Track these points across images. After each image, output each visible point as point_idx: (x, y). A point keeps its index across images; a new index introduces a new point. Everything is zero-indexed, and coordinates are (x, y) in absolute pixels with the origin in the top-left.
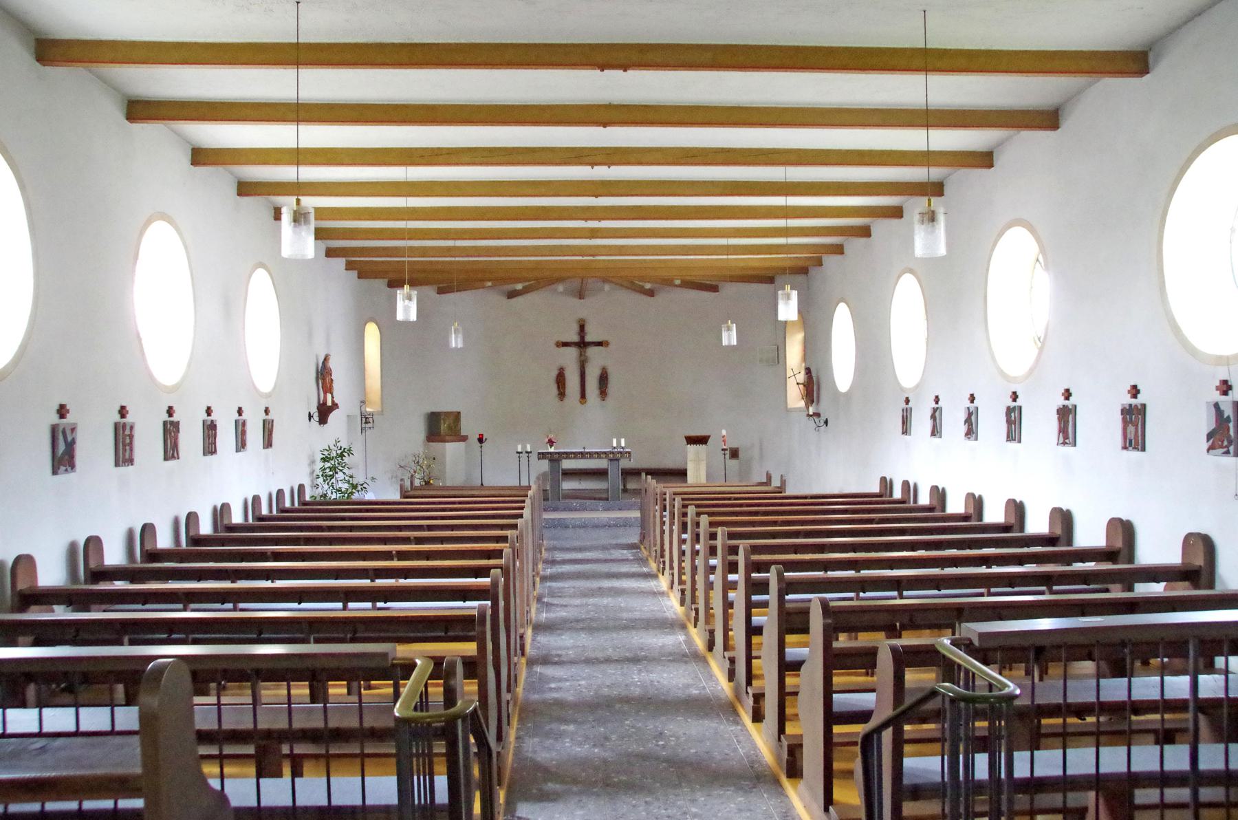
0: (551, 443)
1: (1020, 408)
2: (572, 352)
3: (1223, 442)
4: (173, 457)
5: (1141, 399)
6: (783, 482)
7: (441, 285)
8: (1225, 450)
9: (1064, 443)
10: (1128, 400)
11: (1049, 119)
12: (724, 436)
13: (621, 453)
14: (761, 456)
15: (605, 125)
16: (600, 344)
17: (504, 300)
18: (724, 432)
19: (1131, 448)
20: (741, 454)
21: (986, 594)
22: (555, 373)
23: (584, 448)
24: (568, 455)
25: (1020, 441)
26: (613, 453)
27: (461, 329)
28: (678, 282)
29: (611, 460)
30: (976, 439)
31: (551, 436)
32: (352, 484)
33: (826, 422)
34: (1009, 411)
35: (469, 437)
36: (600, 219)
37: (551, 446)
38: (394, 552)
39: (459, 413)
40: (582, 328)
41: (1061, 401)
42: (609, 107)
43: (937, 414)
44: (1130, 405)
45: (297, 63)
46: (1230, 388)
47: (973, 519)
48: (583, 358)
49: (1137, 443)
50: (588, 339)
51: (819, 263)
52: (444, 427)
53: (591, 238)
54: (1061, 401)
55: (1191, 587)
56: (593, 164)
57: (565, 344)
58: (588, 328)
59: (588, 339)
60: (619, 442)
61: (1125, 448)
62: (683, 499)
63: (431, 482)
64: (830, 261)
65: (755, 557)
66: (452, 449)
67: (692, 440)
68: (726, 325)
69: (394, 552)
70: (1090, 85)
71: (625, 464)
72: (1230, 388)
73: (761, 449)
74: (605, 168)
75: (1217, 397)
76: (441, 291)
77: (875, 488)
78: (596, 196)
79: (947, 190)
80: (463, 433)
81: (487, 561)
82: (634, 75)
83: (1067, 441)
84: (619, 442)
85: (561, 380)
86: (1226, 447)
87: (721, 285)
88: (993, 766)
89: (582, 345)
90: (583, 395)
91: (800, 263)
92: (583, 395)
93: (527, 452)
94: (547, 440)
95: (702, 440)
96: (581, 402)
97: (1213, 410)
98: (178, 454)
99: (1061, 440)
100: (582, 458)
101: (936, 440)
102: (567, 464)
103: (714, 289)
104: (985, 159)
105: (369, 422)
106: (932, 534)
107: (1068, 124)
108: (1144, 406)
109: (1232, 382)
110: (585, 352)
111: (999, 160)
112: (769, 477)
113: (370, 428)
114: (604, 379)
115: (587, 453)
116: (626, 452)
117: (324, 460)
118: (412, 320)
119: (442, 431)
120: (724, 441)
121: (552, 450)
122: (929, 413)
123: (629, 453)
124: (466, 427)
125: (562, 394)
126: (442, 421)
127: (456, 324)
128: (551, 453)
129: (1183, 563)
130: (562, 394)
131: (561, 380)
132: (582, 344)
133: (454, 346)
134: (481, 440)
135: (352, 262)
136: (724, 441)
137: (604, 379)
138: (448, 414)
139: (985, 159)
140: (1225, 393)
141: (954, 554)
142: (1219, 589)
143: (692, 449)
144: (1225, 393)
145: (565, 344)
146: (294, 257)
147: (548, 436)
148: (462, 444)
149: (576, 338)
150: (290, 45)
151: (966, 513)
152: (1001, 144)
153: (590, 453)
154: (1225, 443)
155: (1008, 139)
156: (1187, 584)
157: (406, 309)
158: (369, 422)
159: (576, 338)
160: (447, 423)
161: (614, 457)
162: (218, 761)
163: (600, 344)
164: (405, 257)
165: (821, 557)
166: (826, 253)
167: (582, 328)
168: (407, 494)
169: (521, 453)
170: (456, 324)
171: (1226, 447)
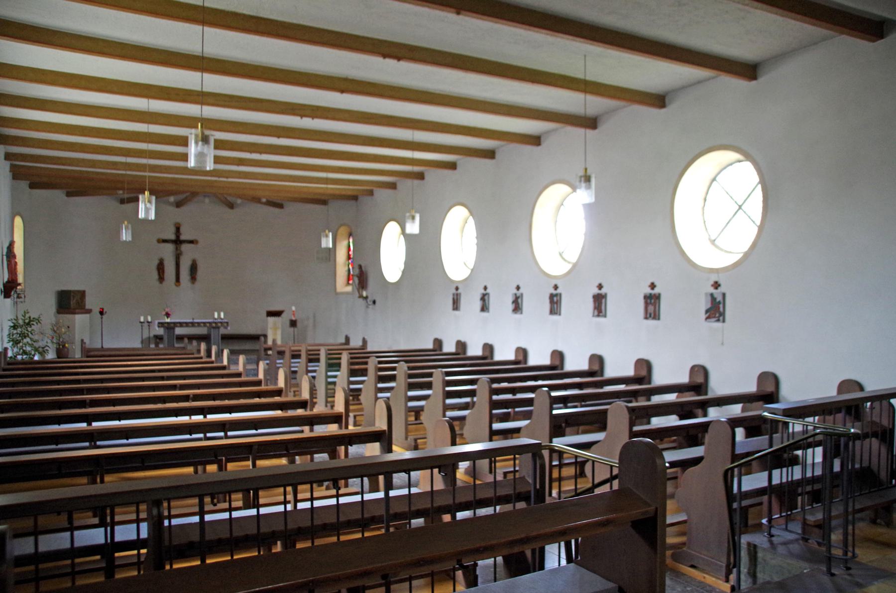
0: (168, 315)
1: (560, 295)
2: (170, 247)
3: (715, 314)
4: (556, 314)
5: (656, 291)
6: (365, 342)
7: (70, 190)
8: (717, 319)
9: (598, 316)
10: (648, 291)
11: (591, 123)
12: (294, 311)
13: (221, 323)
14: (315, 326)
15: (342, 92)
16: (191, 242)
17: (118, 204)
18: (294, 308)
19: (650, 318)
20: (298, 324)
21: (579, 406)
22: (156, 262)
23: (193, 319)
24: (181, 324)
25: (560, 314)
26: (216, 323)
27: (130, 226)
28: (264, 200)
29: (167, 328)
30: (521, 313)
31: (167, 310)
32: (35, 347)
33: (374, 302)
34: (552, 296)
35: (93, 310)
36: (261, 153)
37: (168, 317)
38: (191, 396)
39: (84, 292)
40: (178, 229)
41: (483, 291)
42: (346, 80)
43: (486, 297)
44: (651, 294)
45: (203, 22)
46: (719, 285)
47: (242, 376)
48: (179, 252)
49: (655, 315)
50: (183, 238)
51: (371, 193)
52: (73, 303)
53: (238, 165)
54: (596, 291)
55: (695, 395)
56: (302, 116)
57: (165, 241)
58: (182, 230)
59: (183, 238)
60: (219, 315)
61: (646, 318)
62: (350, 354)
63: (67, 345)
64: (381, 194)
65: (495, 386)
66: (79, 319)
67: (271, 314)
68: (324, 234)
69: (191, 396)
70: (624, 107)
71: (223, 331)
72: (719, 285)
73: (314, 321)
74: (298, 118)
75: (712, 290)
76: (69, 194)
77: (430, 346)
78: (279, 137)
79: (497, 156)
80: (88, 307)
81: (213, 402)
82: (404, 65)
83: (601, 314)
84: (219, 315)
85: (161, 268)
86: (717, 317)
87: (285, 204)
88: (802, 490)
89: (178, 242)
90: (178, 279)
91: (355, 193)
92: (178, 279)
93: (148, 322)
94: (164, 313)
95: (277, 314)
96: (176, 285)
97: (709, 298)
98: (560, 312)
99: (596, 313)
100: (198, 326)
101: (485, 314)
102: (179, 331)
103: (280, 206)
104: (535, 140)
105: (21, 298)
106: (199, 389)
107: (603, 128)
108: (659, 295)
109: (656, 283)
110: (180, 247)
111: (545, 144)
112: (347, 339)
113: (22, 302)
114: (194, 268)
115: (196, 323)
116: (225, 322)
117: (15, 327)
118: (150, 219)
119: (72, 306)
120: (294, 315)
121: (168, 320)
122: (479, 297)
123: (227, 323)
124: (89, 303)
125: (161, 279)
126: (72, 298)
127: (126, 223)
128: (168, 323)
129: (690, 382)
130: (161, 279)
131: (161, 268)
132: (178, 242)
133: (124, 239)
134: (102, 313)
135: (16, 165)
136: (294, 315)
137: (194, 268)
138: (79, 291)
139: (535, 140)
140: (716, 288)
141: (505, 386)
142: (710, 395)
143: (271, 320)
144: (716, 288)
145: (165, 241)
146: (198, 169)
147: (165, 310)
148: (88, 316)
149: (173, 237)
150: (199, 6)
151: (516, 359)
152: (548, 133)
153: (198, 323)
154: (717, 315)
155: (554, 130)
156: (692, 393)
157: (147, 210)
158: (21, 298)
159: (173, 237)
160: (75, 299)
161: (215, 326)
162: (136, 567)
163: (191, 242)
164: (146, 172)
165: (128, 409)
166: (377, 187)
167: (178, 229)
168: (89, 354)
169: (144, 322)
170: (126, 223)
171: (717, 317)
